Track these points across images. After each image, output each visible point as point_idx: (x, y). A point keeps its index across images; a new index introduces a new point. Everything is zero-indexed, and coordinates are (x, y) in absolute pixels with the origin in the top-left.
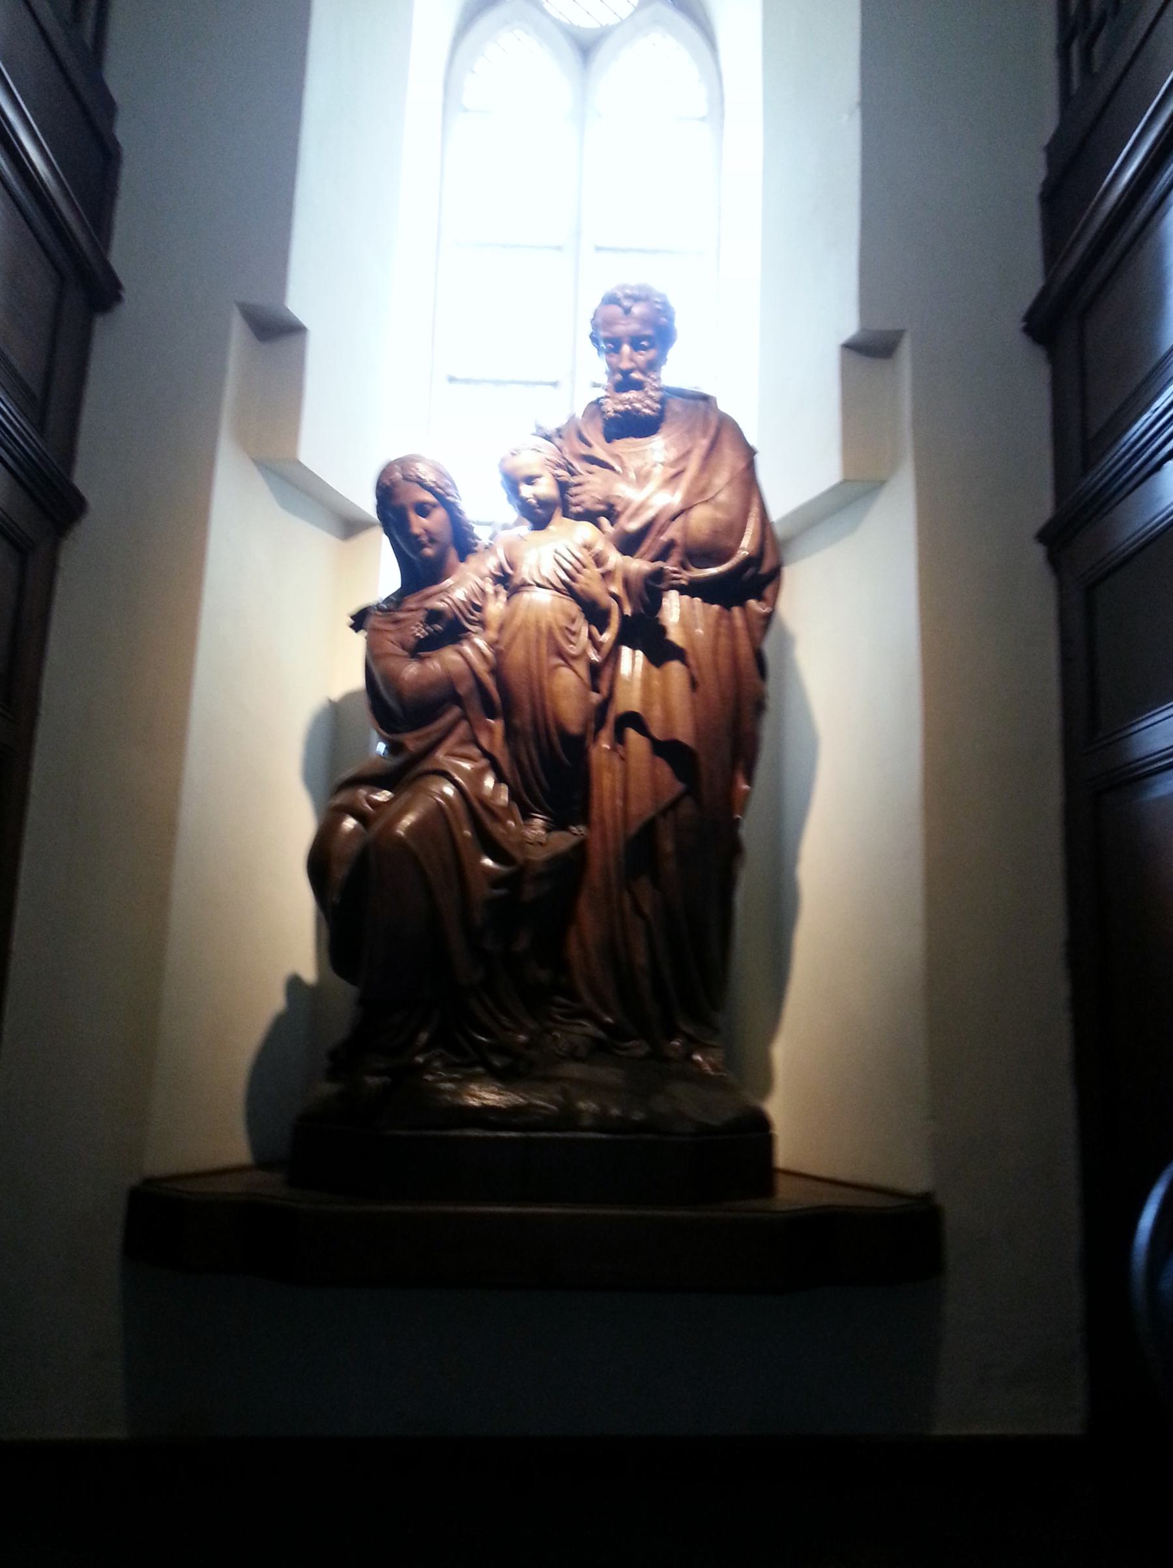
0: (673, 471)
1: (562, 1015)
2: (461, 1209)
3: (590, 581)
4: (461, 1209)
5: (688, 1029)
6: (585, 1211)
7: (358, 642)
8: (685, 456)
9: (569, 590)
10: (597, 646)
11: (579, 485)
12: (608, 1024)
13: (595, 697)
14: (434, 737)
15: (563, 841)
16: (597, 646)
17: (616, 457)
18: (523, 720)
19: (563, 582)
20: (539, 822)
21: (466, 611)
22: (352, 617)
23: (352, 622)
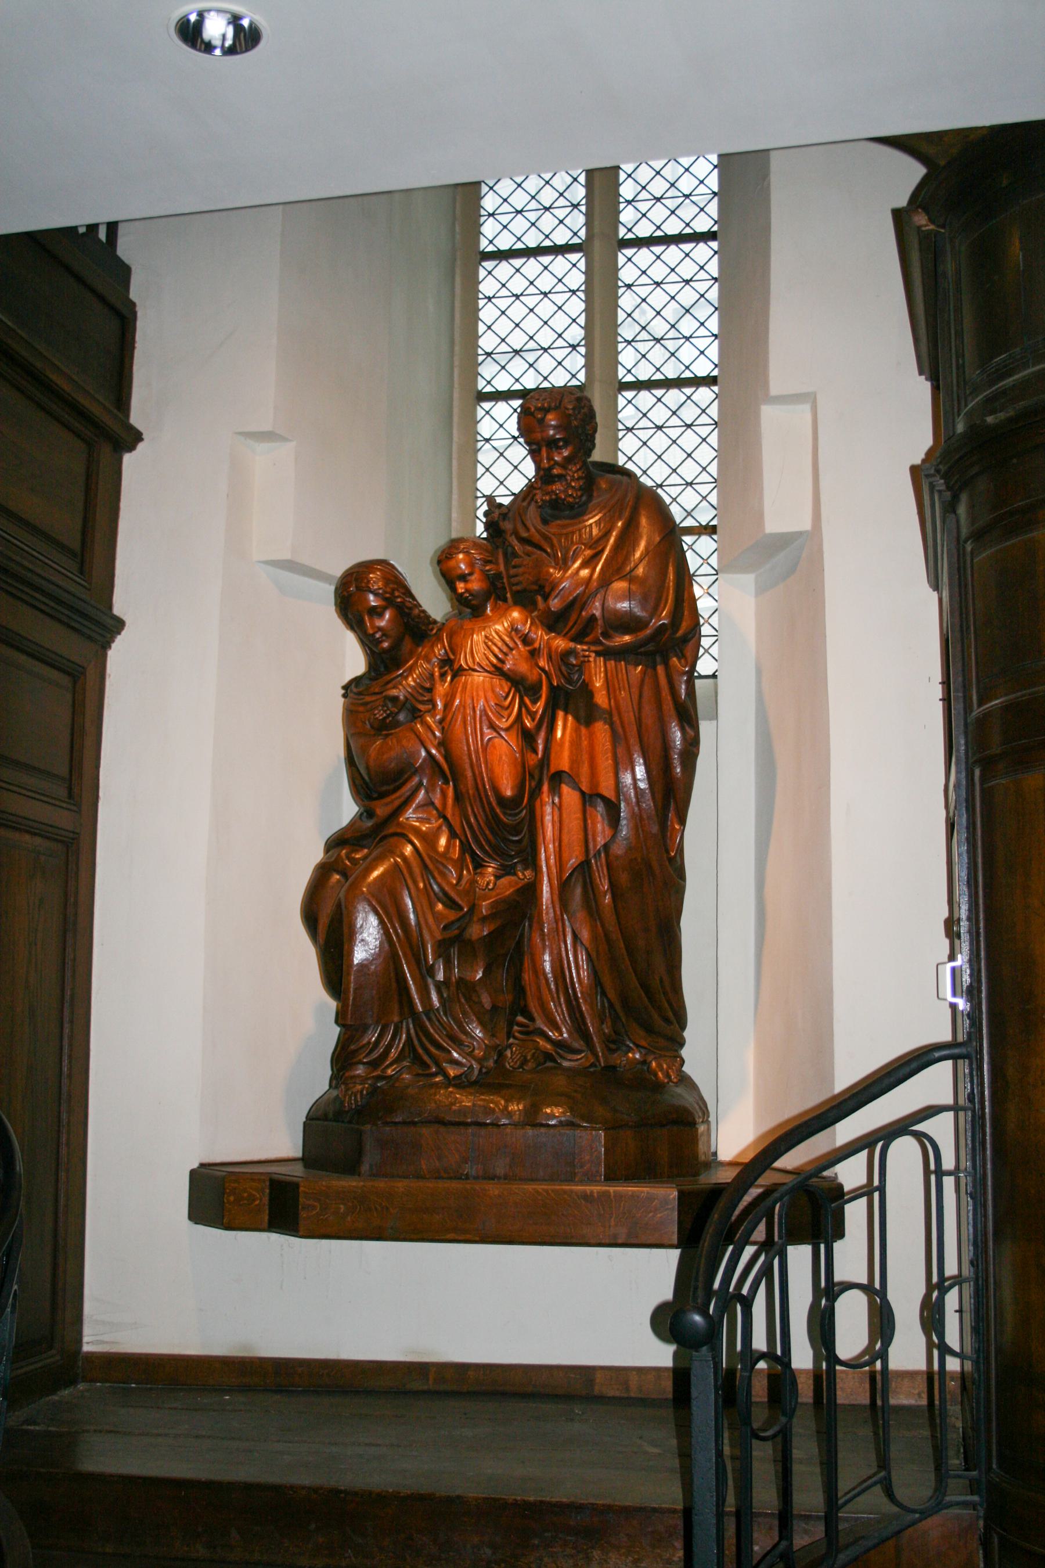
1: (520, 1032)
6: (413, 987)
9: (498, 670)
10: (532, 715)
13: (532, 760)
14: (397, 803)
15: (508, 886)
16: (532, 715)
17: (546, 538)
19: (494, 665)
21: (416, 695)
23: (343, 692)
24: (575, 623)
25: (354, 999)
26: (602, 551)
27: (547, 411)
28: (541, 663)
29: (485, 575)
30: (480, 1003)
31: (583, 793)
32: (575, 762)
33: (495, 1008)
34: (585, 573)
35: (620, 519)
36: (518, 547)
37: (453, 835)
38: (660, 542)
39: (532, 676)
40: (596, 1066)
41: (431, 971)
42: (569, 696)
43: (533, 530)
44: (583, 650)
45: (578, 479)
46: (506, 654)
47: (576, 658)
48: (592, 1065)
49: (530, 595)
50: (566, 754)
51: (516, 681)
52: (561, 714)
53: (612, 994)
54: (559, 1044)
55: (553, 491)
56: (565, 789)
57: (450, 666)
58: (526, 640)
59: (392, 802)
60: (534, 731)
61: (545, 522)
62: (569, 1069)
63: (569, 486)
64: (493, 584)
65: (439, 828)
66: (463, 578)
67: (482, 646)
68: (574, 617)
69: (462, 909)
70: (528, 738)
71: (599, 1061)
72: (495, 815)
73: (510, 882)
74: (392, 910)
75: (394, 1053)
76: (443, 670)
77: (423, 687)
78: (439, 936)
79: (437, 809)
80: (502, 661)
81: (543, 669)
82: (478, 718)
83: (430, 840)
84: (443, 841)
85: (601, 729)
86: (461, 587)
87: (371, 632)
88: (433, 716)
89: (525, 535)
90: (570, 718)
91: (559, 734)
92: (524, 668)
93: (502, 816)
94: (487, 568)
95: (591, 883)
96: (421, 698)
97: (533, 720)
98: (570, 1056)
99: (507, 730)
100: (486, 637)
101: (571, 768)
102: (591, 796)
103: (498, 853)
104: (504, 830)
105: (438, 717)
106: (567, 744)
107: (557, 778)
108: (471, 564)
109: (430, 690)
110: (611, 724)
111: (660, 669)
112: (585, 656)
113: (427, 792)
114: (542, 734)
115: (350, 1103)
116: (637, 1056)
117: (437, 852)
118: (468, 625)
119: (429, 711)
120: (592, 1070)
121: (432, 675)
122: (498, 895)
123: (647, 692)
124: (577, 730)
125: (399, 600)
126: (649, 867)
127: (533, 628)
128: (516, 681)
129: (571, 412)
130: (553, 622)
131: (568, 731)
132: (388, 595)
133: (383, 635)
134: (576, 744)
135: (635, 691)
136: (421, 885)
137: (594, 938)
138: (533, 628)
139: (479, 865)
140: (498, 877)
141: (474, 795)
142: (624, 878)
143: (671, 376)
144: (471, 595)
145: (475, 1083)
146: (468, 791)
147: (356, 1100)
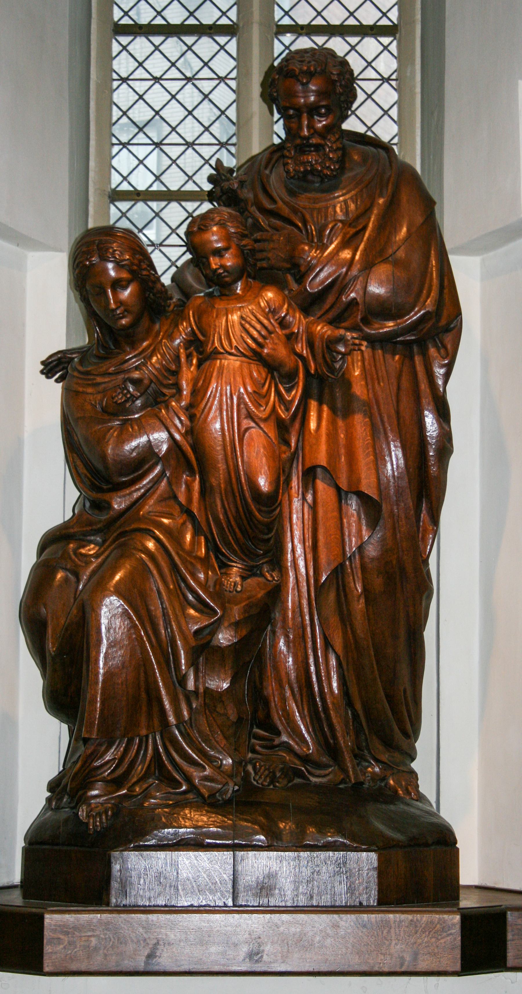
0: (352, 231)
2: (214, 841)
3: (275, 349)
4: (214, 841)
5: (385, 757)
7: (53, 391)
8: (365, 212)
9: (256, 356)
10: (287, 405)
11: (262, 251)
12: (330, 743)
16: (287, 405)
17: (295, 211)
18: (218, 479)
20: (236, 570)
21: (160, 378)
22: (43, 363)
23: (42, 367)
24: (332, 307)
25: (102, 710)
26: (365, 228)
27: (311, 75)
28: (298, 348)
29: (241, 251)
30: (226, 715)
31: (338, 489)
32: (332, 455)
33: (240, 720)
34: (346, 254)
35: (381, 196)
36: (262, 220)
37: (197, 531)
38: (422, 224)
39: (289, 362)
40: (346, 783)
41: (183, 681)
42: (326, 384)
43: (280, 203)
44: (353, 338)
45: (335, 150)
46: (264, 338)
47: (346, 346)
48: (343, 781)
49: (286, 272)
50: (323, 448)
51: (271, 366)
52: (313, 404)
53: (358, 706)
54: (306, 759)
55: (308, 162)
56: (320, 485)
57: (201, 348)
58: (283, 323)
59: (131, 494)
60: (288, 422)
61: (292, 193)
62: (316, 785)
63: (326, 155)
64: (245, 260)
65: (184, 523)
66: (218, 253)
67: (238, 328)
68: (330, 299)
69: (216, 613)
70: (283, 428)
71: (348, 776)
72: (249, 513)
73: (258, 584)
74: (143, 612)
75: (140, 769)
76: (188, 351)
77: (168, 370)
78: (193, 643)
79: (180, 504)
80: (261, 345)
81: (300, 356)
82: (235, 407)
83: (175, 535)
84: (188, 537)
85: (359, 420)
86: (214, 262)
87: (113, 306)
88: (179, 401)
89: (269, 205)
90: (325, 408)
91: (313, 425)
92: (282, 352)
93: (257, 513)
94: (244, 242)
95: (344, 586)
96: (165, 382)
97: (288, 409)
98: (318, 772)
99: (265, 420)
100: (242, 318)
101: (329, 462)
102: (347, 493)
103: (247, 554)
104: (250, 529)
105: (183, 404)
106: (324, 439)
107: (310, 475)
108: (228, 237)
109: (176, 373)
110: (371, 417)
111: (418, 360)
112: (354, 344)
113: (169, 483)
114: (297, 425)
115: (95, 825)
116: (377, 769)
117: (183, 549)
118: (220, 305)
119: (173, 396)
120: (341, 786)
121: (178, 357)
122: (249, 598)
123: (405, 383)
124: (333, 423)
125: (144, 273)
126: (402, 570)
127: (291, 311)
128: (271, 366)
129: (335, 78)
130: (309, 304)
131: (324, 423)
132: (135, 267)
133: (126, 310)
134: (332, 436)
135: (394, 381)
136: (171, 587)
137: (346, 647)
138: (291, 311)
139: (224, 566)
140: (243, 578)
141: (226, 490)
142: (378, 582)
143: (301, 22)
144: (225, 271)
145: (228, 802)
146: (219, 484)
147: (101, 822)
